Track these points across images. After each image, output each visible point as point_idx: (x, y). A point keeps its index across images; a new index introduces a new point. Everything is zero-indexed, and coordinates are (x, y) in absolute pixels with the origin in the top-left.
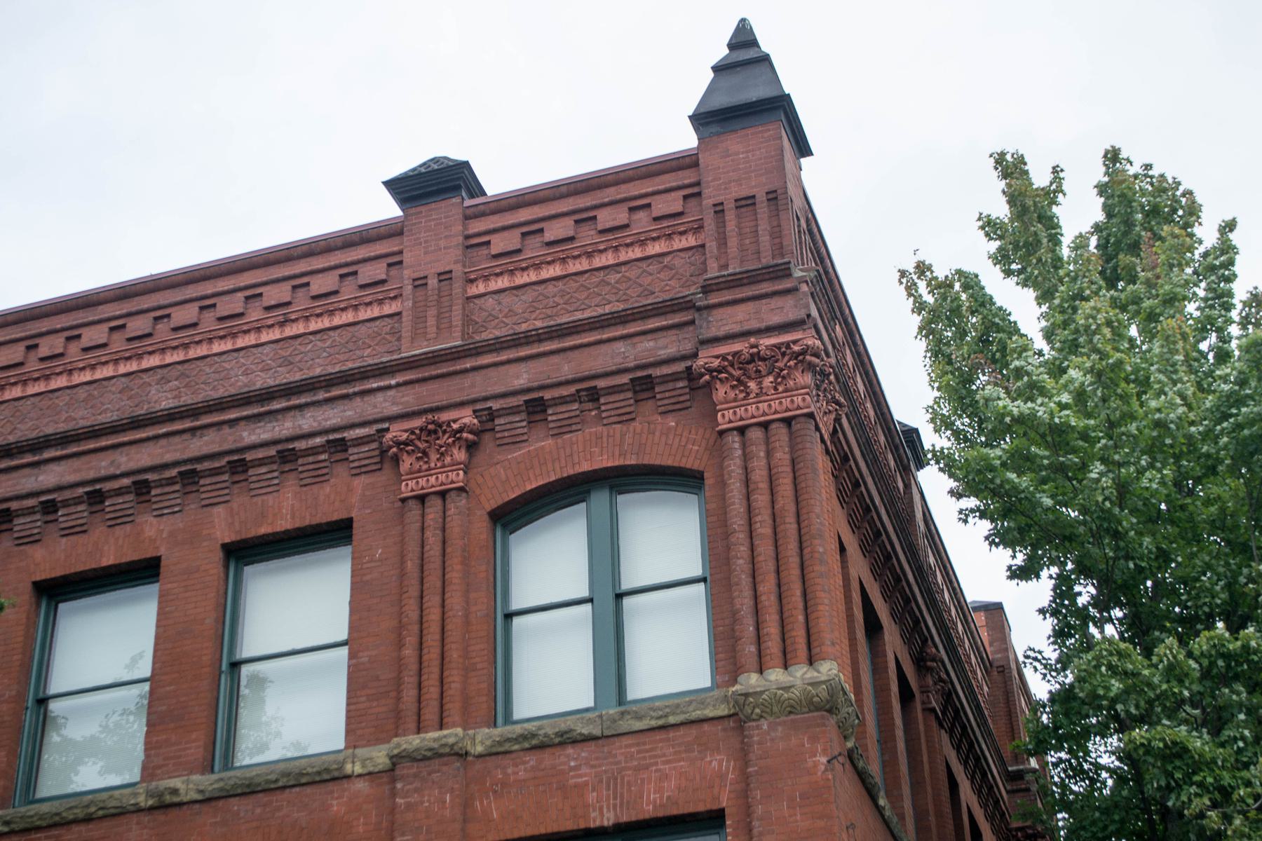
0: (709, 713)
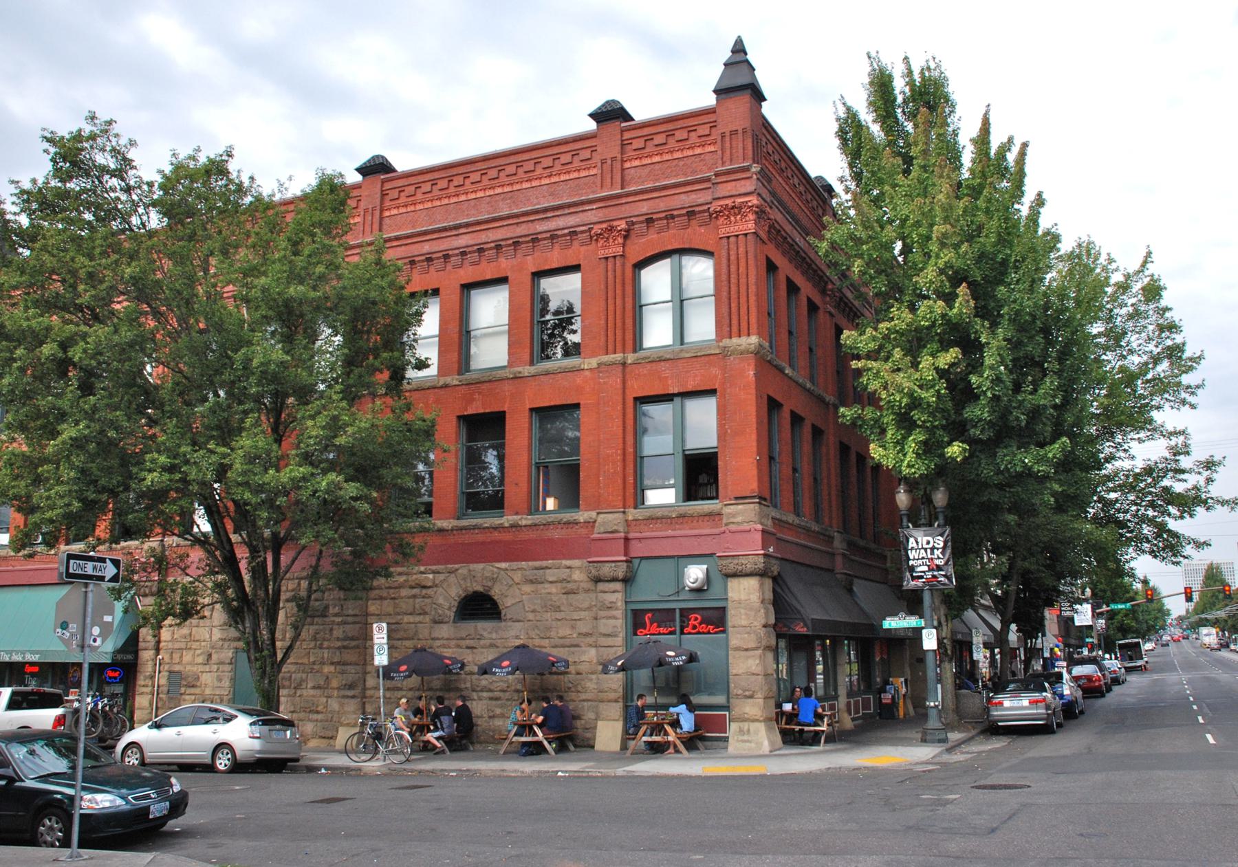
0: (713, 352)
